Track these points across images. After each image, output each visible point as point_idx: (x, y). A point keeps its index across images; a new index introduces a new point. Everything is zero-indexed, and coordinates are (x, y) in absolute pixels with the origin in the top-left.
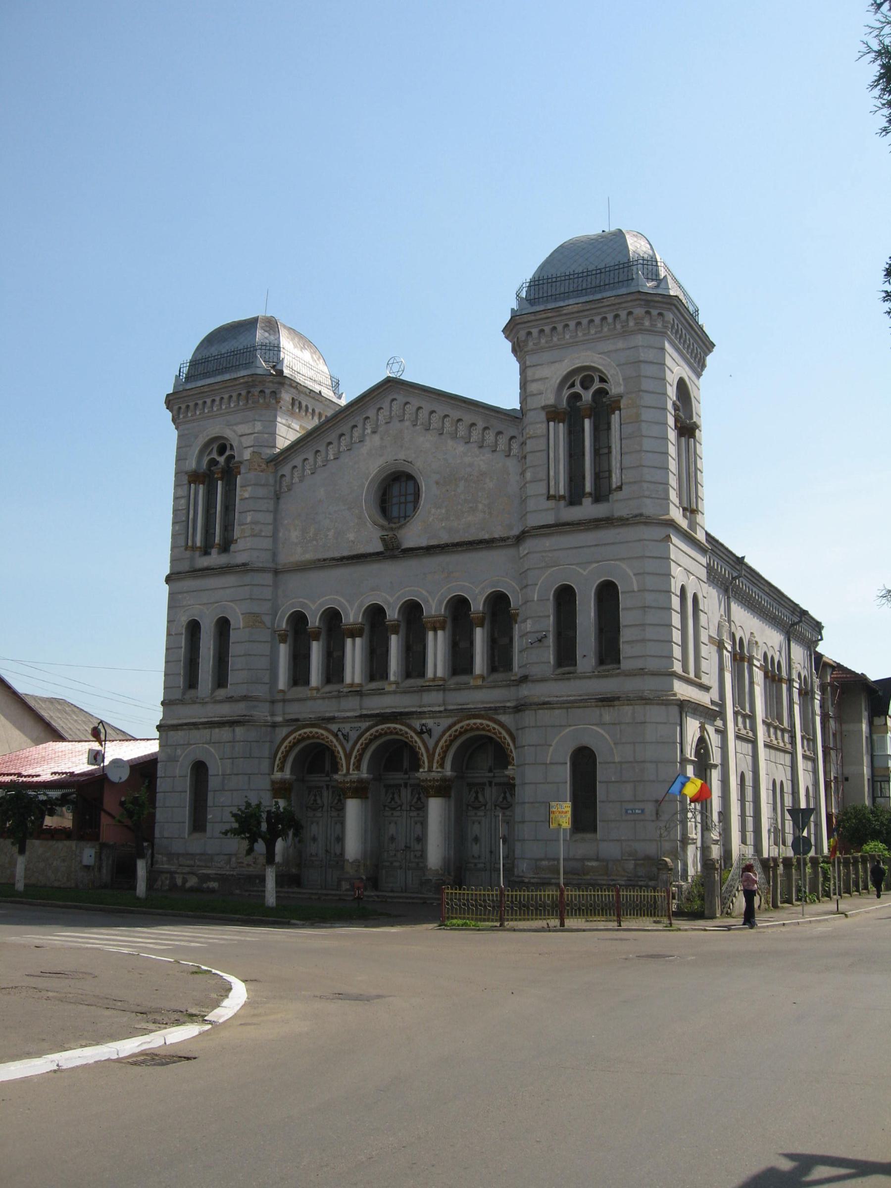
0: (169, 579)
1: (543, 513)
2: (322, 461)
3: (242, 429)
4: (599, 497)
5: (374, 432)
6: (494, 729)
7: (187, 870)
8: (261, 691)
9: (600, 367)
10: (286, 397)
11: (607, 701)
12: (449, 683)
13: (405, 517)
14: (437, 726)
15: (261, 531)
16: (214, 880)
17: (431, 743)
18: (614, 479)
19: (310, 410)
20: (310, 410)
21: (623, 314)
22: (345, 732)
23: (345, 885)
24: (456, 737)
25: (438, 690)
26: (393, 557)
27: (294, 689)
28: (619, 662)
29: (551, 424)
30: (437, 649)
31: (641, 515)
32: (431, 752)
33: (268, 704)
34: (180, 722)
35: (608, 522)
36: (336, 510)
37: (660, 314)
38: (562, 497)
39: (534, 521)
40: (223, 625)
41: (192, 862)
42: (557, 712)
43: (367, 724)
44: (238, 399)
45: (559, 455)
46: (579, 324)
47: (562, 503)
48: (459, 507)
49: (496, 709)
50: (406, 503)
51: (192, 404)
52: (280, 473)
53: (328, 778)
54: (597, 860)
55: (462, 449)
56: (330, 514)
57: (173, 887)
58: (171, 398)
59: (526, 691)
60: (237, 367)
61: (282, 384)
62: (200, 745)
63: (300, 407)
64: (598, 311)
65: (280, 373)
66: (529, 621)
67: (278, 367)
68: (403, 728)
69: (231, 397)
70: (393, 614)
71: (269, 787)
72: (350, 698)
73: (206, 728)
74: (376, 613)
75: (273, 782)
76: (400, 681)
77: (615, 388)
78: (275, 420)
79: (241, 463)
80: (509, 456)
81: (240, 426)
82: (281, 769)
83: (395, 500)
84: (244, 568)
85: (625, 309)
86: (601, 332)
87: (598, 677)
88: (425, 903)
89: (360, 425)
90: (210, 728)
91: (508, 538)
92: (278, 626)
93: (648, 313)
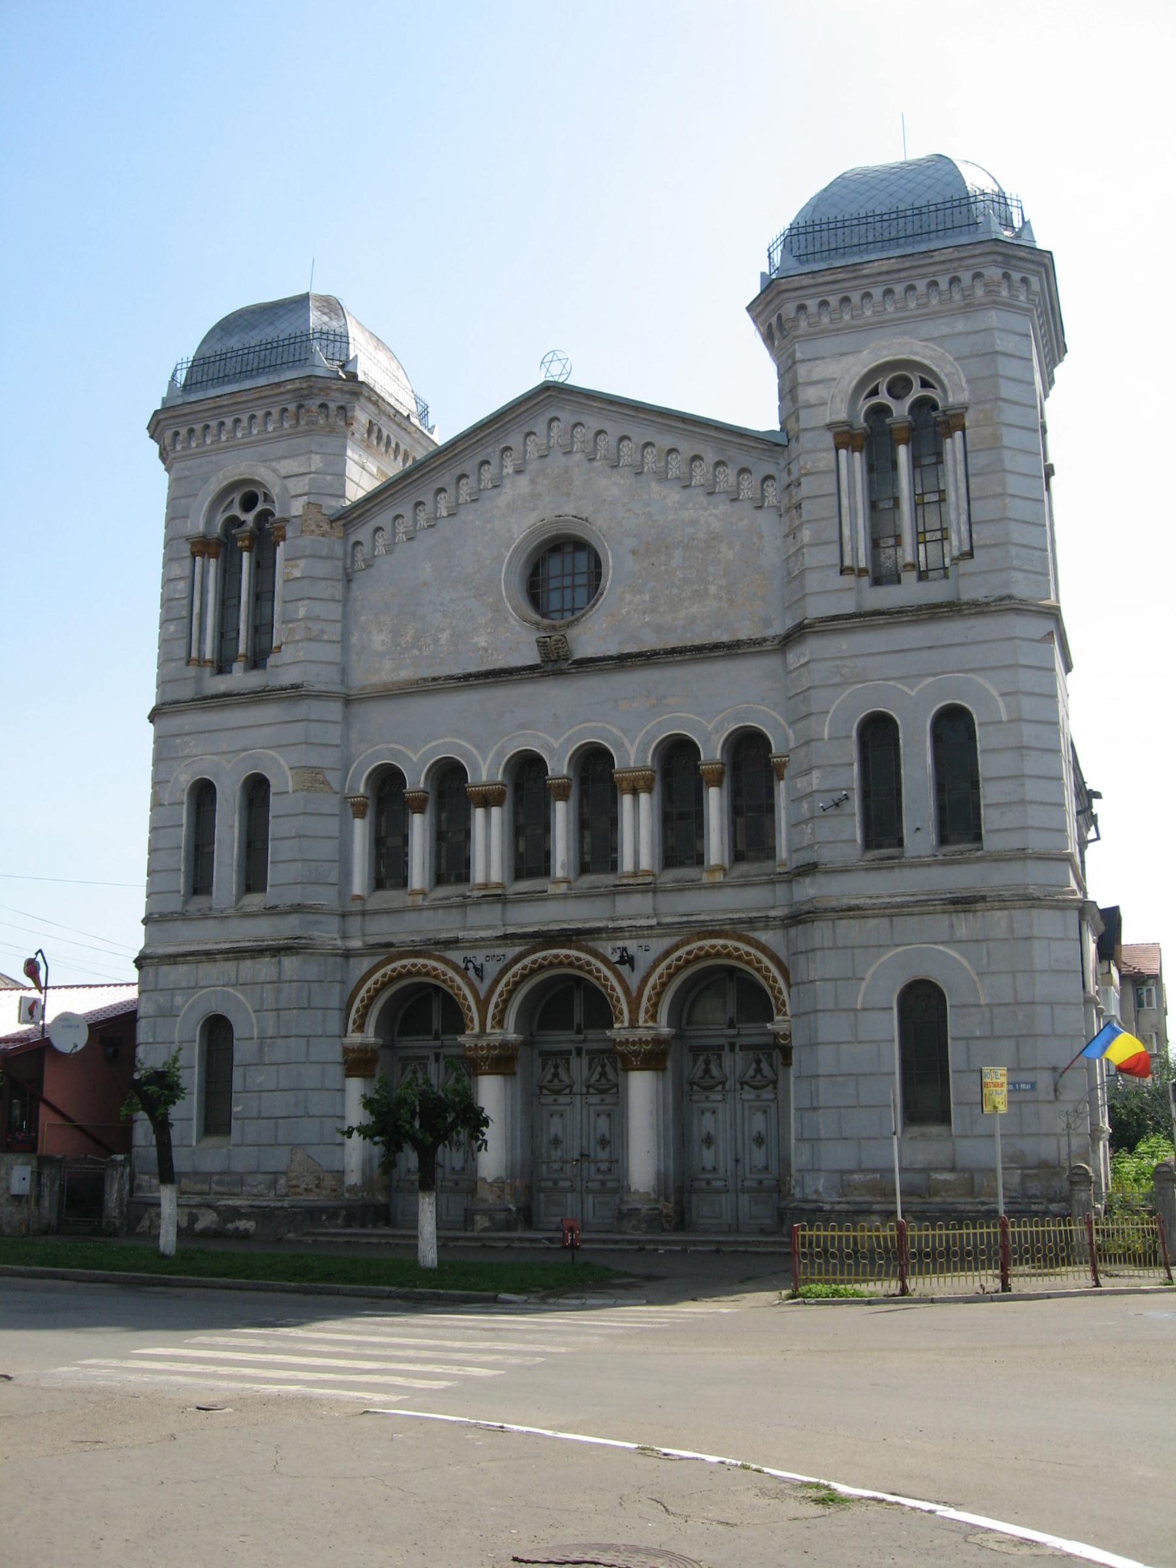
0: (154, 716)
1: (830, 595)
2: (427, 520)
3: (288, 466)
5: (519, 472)
6: (748, 954)
7: (197, 1199)
8: (325, 897)
9: (926, 362)
10: (362, 416)
11: (964, 903)
12: (661, 880)
13: (573, 610)
14: (646, 951)
16: (247, 1216)
17: (634, 980)
19: (393, 445)
20: (393, 445)
21: (966, 277)
22: (478, 963)
23: (481, 1221)
24: (679, 969)
25: (643, 892)
26: (560, 673)
27: (380, 894)
29: (843, 452)
30: (638, 826)
31: (1010, 597)
32: (634, 994)
33: (337, 919)
35: (952, 609)
36: (456, 596)
37: (1024, 280)
38: (862, 572)
39: (816, 608)
40: (257, 790)
41: (205, 1187)
42: (872, 923)
43: (518, 950)
44: (282, 419)
45: (856, 503)
46: (889, 292)
47: (866, 580)
48: (675, 591)
50: (573, 587)
51: (198, 427)
52: (353, 539)
53: (438, 1043)
54: (953, 1169)
55: (677, 497)
56: (441, 604)
58: (162, 416)
60: (273, 368)
61: (356, 394)
63: (379, 438)
64: (922, 271)
65: (353, 377)
66: (816, 774)
67: (349, 368)
68: (582, 955)
69: (268, 414)
70: (559, 767)
71: (339, 1057)
72: (484, 907)
73: (227, 960)
74: (527, 766)
75: (346, 1050)
76: (572, 877)
77: (955, 392)
78: (344, 454)
79: (287, 520)
80: (760, 507)
81: (283, 462)
82: (360, 1028)
83: (554, 583)
84: (295, 693)
85: (968, 268)
86: (925, 305)
87: (944, 863)
88: (643, 1249)
89: (495, 461)
90: (235, 959)
91: (765, 640)
92: (350, 789)
93: (1006, 276)
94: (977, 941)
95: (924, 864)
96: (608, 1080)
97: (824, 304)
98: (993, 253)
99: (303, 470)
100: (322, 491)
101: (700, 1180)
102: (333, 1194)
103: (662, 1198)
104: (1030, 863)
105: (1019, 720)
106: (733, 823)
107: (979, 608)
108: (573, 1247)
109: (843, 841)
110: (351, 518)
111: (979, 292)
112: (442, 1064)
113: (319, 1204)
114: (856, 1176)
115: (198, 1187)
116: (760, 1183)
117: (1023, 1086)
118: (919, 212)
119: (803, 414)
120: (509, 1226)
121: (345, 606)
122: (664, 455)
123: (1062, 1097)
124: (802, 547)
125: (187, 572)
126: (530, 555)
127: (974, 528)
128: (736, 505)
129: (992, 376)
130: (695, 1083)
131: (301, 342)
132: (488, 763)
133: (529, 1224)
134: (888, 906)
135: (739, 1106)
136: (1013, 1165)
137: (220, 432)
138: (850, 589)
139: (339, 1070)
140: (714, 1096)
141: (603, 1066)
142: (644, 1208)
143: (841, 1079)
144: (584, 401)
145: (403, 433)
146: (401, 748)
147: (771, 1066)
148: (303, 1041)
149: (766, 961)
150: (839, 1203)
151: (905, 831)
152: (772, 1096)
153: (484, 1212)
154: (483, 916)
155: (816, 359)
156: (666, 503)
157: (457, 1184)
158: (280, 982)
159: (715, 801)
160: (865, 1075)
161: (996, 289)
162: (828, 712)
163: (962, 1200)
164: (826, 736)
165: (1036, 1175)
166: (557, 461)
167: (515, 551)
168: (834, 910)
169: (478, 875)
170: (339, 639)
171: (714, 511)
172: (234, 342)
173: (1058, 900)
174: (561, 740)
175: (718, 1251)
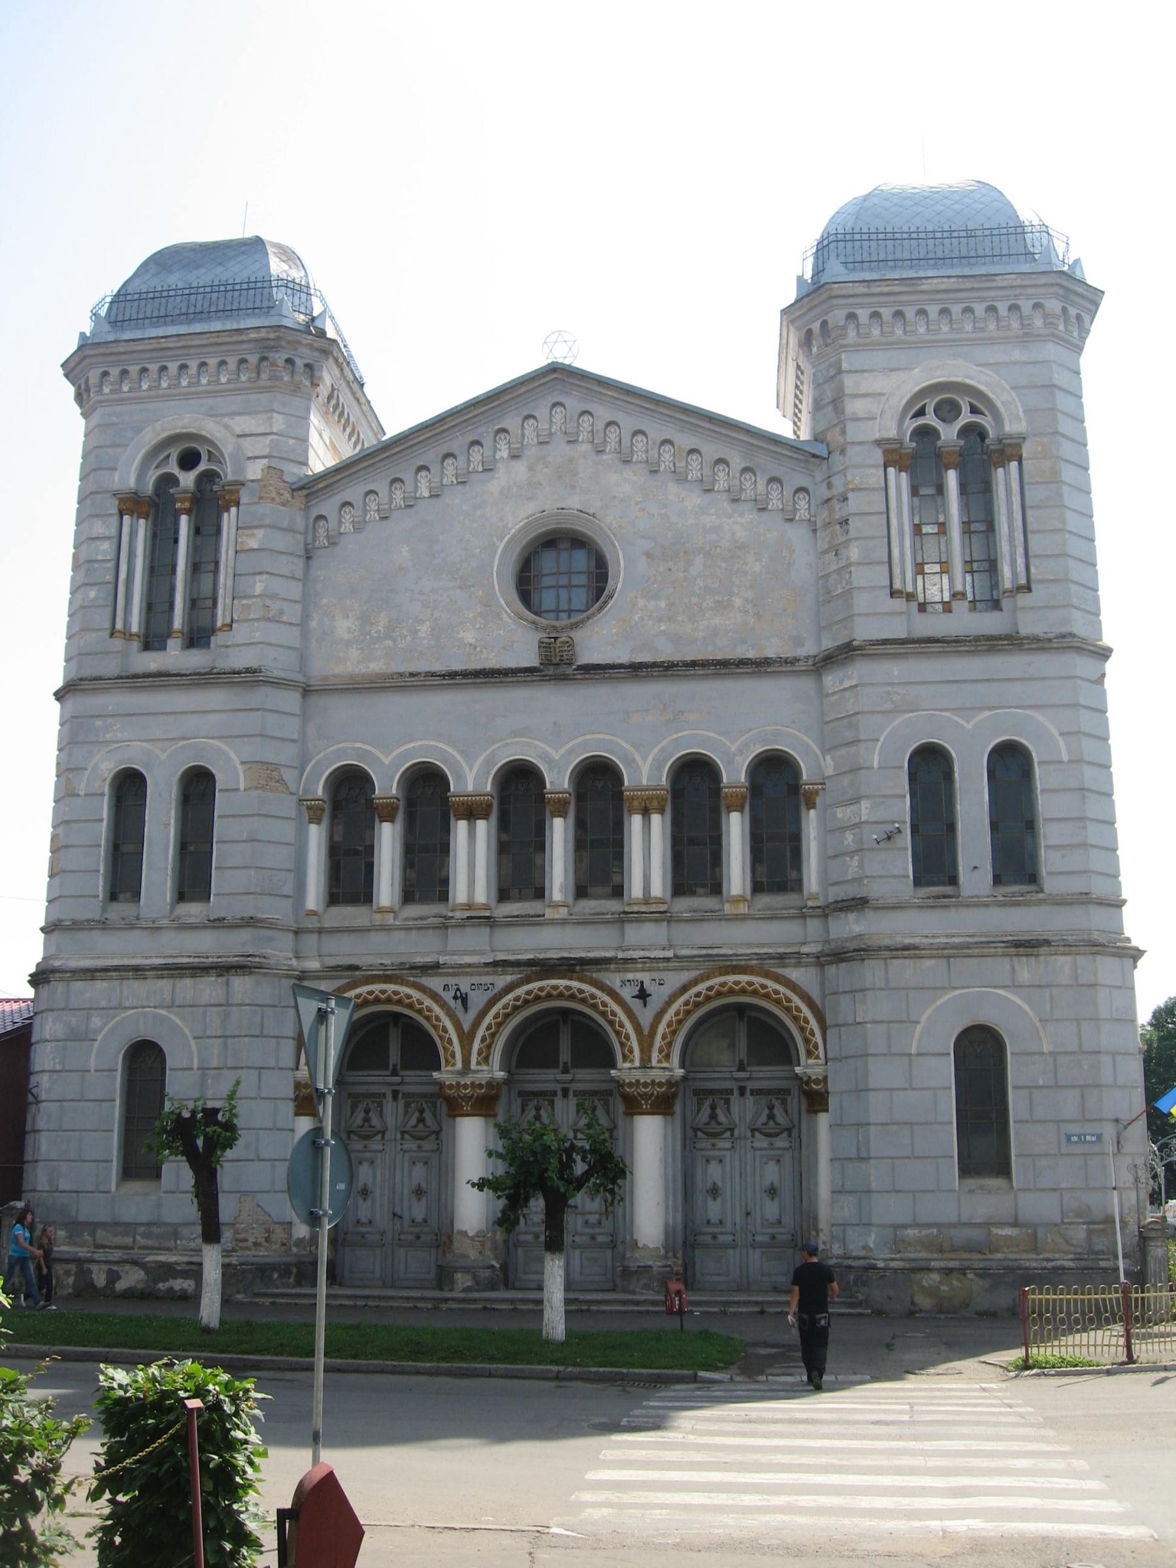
3: (242, 424)
4: (197, 637)
5: (515, 457)
6: (776, 992)
7: (117, 1255)
8: (278, 910)
9: (982, 388)
10: (328, 377)
11: (1026, 946)
15: (281, 612)
17: (646, 1017)
18: (1006, 571)
23: (462, 1280)
25: (656, 920)
26: (564, 678)
27: (335, 910)
28: (953, 880)
32: (646, 1032)
33: (291, 935)
34: (100, 963)
39: (864, 631)
40: (198, 786)
41: (128, 1241)
42: (929, 963)
43: (509, 979)
48: (695, 600)
49: (781, 957)
50: (569, 587)
51: (134, 369)
52: (315, 512)
53: (397, 1079)
54: (1015, 1224)
57: (85, 1290)
59: (850, 927)
61: (326, 353)
62: (145, 1010)
64: (979, 294)
65: (322, 333)
66: (865, 804)
68: (585, 987)
73: (162, 977)
78: (307, 418)
80: (791, 520)
81: (238, 419)
83: (547, 581)
85: (1028, 297)
86: (983, 330)
88: (724, 1313)
90: (171, 977)
91: (796, 660)
92: (306, 791)
94: (1039, 986)
95: (979, 908)
96: (426, 1126)
97: (876, 315)
98: (1052, 285)
99: (261, 430)
100: (285, 456)
101: (705, 1234)
102: (283, 1249)
103: (670, 1254)
104: (1093, 909)
105: (1080, 761)
106: (578, 860)
107: (1039, 644)
108: (681, 1312)
109: (894, 877)
110: (313, 488)
111: (1038, 322)
112: (401, 1103)
113: (269, 1260)
114: (910, 1232)
115: (119, 1240)
116: (773, 1237)
117: (1088, 1138)
118: (970, 234)
119: (850, 426)
120: (493, 1287)
121: (304, 585)
122: (685, 455)
123: (1123, 1151)
124: (849, 565)
125: (113, 531)
126: (524, 548)
127: (1032, 561)
128: (765, 515)
129: (1049, 409)
130: (699, 1129)
131: (262, 285)
132: (475, 770)
133: (508, 1284)
134: (946, 946)
135: (749, 1156)
136: (1079, 1220)
137: (199, 374)
138: (901, 613)
139: (290, 1107)
140: (721, 1144)
141: (422, 1111)
142: (656, 1265)
143: (894, 1127)
144: (596, 388)
145: (355, 403)
146: (369, 748)
147: (434, 1115)
148: (256, 1072)
149: (797, 1001)
150: (892, 1260)
151: (961, 868)
152: (786, 1144)
153: (466, 1270)
154: (469, 940)
155: (864, 371)
156: (686, 507)
157: (418, 1237)
158: (228, 1005)
159: (559, 832)
160: (921, 1124)
161: (1055, 321)
162: (878, 740)
163: (1024, 1256)
164: (876, 765)
165: (1104, 1230)
166: (559, 450)
167: (509, 542)
168: (888, 948)
169: (459, 893)
170: (298, 622)
171: (739, 519)
172: (174, 280)
173: (1119, 948)
174: (562, 751)
175: (762, 1312)
